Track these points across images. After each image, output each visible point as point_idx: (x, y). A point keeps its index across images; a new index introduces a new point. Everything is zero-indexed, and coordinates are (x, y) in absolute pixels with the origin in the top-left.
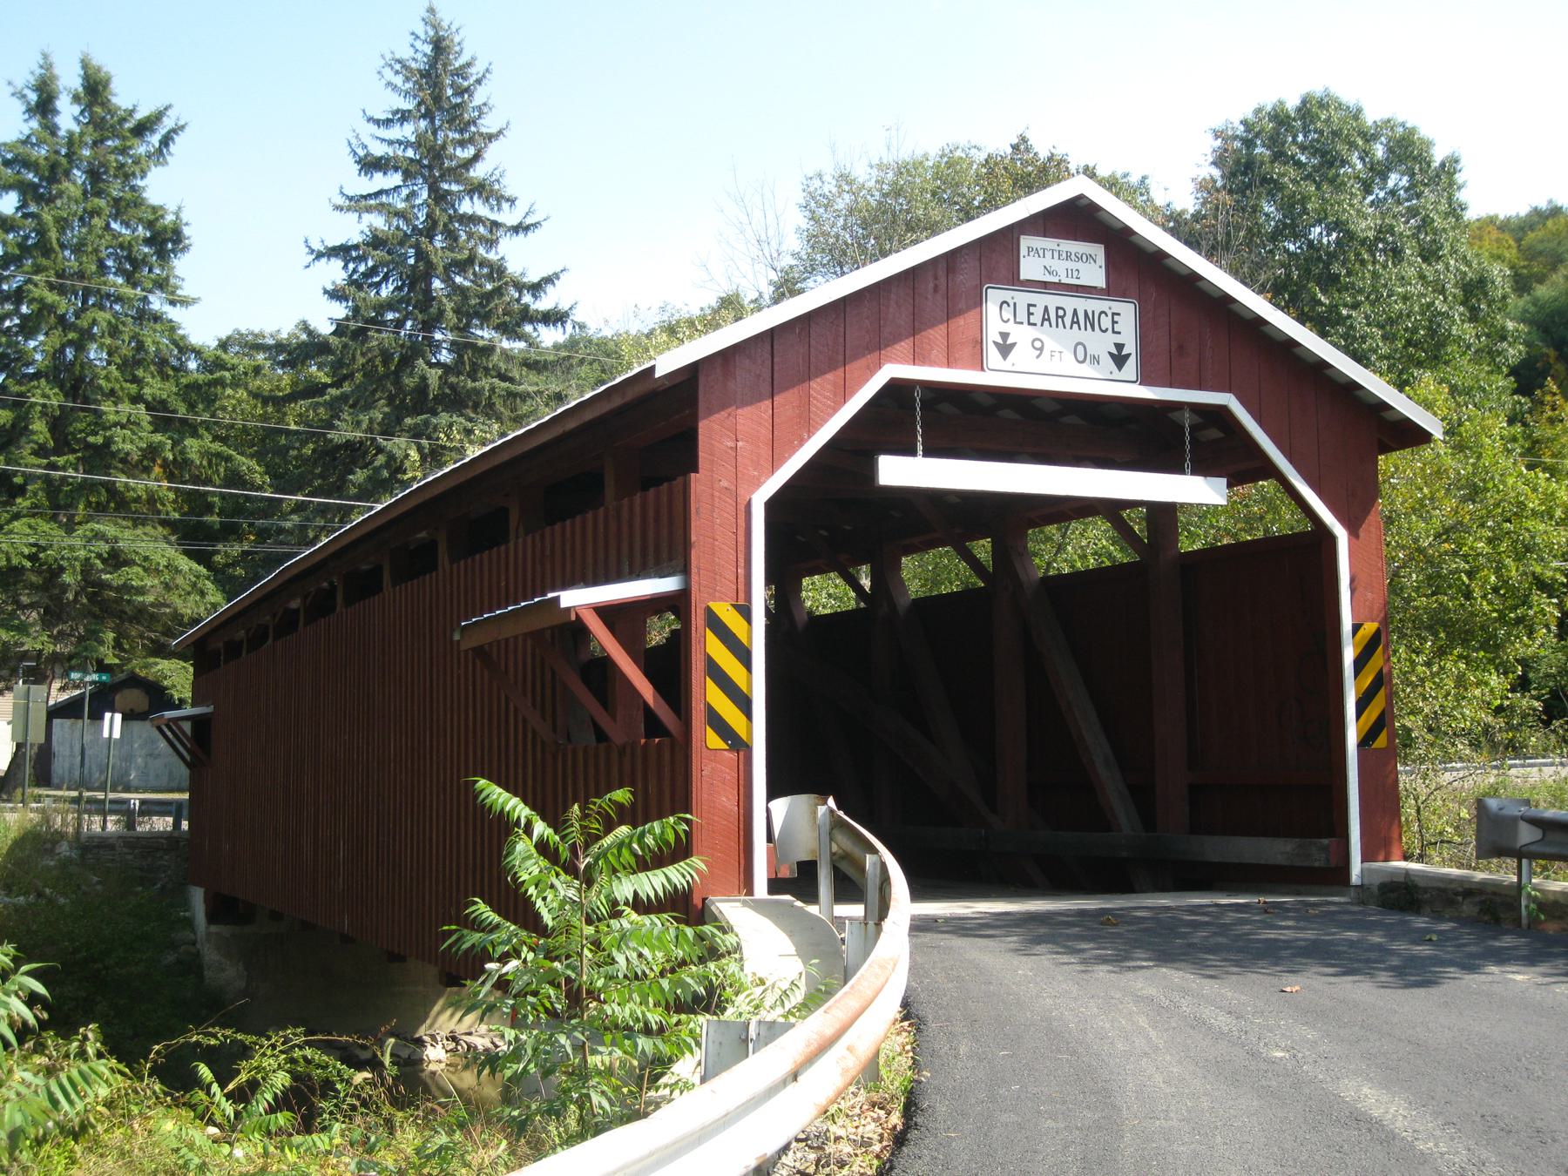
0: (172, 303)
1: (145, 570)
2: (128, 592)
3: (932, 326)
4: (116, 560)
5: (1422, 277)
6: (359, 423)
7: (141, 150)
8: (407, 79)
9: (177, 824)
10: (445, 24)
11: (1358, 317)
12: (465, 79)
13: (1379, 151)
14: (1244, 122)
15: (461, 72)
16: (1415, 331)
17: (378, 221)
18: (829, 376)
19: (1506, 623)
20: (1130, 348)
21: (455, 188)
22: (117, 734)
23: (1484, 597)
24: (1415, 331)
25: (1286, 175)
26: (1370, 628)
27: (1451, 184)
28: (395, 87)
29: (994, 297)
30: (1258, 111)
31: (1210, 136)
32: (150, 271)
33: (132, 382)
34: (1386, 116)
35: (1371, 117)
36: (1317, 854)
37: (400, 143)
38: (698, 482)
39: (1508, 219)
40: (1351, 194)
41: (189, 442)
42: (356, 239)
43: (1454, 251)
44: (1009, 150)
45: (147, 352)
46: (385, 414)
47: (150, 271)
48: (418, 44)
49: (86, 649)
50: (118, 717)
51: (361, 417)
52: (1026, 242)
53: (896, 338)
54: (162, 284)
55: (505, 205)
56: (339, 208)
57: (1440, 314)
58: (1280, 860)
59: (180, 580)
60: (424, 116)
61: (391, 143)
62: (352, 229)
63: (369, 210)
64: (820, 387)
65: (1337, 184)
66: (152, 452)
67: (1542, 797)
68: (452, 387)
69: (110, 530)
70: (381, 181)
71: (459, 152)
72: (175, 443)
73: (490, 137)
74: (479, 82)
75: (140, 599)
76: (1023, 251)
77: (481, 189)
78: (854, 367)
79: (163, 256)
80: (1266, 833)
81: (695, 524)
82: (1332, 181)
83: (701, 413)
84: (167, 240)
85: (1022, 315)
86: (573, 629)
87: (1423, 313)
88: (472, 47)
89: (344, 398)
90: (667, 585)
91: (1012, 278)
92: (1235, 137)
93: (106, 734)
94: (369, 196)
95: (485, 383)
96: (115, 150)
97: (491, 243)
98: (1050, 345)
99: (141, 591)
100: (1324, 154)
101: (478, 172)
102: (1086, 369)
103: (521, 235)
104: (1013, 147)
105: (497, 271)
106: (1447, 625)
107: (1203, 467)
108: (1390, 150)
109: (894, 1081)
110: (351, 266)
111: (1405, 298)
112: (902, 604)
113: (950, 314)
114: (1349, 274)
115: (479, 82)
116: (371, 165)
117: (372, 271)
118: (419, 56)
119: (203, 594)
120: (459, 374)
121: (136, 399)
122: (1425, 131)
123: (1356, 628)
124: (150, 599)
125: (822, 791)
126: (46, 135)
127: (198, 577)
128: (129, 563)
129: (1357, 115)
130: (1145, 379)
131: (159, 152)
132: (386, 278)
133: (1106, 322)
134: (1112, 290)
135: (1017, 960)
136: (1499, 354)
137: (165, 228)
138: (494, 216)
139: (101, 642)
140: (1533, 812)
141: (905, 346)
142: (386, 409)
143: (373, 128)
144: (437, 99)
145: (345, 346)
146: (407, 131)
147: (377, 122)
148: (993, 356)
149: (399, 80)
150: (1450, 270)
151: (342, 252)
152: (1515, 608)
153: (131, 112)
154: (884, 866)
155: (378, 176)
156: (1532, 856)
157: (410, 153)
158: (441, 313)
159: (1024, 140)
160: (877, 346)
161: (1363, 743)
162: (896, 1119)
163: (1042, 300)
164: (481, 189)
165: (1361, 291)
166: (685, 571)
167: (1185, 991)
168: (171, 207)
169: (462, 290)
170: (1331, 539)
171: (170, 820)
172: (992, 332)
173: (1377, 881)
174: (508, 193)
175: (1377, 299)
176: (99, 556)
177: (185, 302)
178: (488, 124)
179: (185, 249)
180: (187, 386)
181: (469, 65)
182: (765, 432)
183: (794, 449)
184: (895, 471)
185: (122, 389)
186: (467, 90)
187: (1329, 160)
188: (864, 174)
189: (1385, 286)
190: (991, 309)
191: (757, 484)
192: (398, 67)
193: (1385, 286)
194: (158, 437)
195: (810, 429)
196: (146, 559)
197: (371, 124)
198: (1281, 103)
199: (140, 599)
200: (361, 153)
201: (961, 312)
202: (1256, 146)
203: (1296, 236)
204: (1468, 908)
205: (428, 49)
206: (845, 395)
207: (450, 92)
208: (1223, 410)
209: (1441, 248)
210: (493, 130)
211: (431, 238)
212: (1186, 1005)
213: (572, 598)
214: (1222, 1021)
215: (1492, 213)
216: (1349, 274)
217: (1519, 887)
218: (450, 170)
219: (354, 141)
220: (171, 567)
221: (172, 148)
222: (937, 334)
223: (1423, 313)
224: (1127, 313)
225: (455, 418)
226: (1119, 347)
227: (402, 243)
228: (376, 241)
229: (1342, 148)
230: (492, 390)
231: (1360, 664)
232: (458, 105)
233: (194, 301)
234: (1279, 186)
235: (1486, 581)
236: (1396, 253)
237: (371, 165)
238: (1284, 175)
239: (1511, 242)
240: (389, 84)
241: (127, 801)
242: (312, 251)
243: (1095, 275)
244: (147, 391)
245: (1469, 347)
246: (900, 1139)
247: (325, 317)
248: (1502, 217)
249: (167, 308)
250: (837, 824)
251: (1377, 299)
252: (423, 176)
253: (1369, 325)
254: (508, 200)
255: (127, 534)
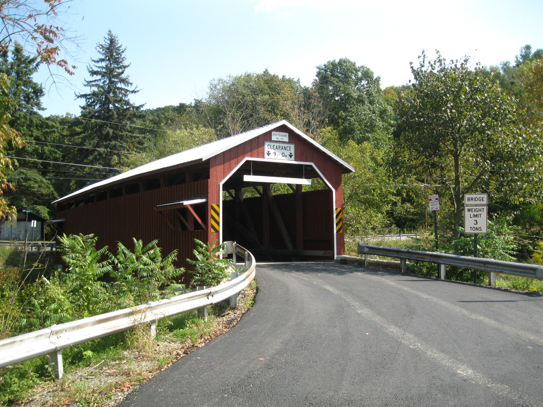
0: (39, 109)
1: (34, 182)
2: (30, 188)
3: (255, 149)
4: (27, 179)
5: (369, 109)
6: (91, 143)
7: (31, 67)
8: (103, 50)
9: (52, 249)
10: (114, 35)
11: (352, 119)
12: (119, 51)
13: (360, 74)
14: (325, 65)
15: (118, 49)
16: (367, 123)
17: (95, 89)
18: (235, 160)
19: (382, 202)
20: (293, 154)
21: (116, 80)
22: (35, 226)
23: (377, 196)
24: (367, 123)
25: (335, 80)
26: (339, 209)
27: (378, 84)
28: (100, 52)
29: (267, 144)
30: (329, 62)
31: (316, 68)
32: (34, 101)
33: (30, 131)
34: (362, 65)
35: (358, 65)
36: (328, 254)
37: (101, 67)
38: (210, 181)
39: (397, 88)
40: (352, 86)
41: (45, 148)
42: (89, 93)
43: (378, 101)
44: (263, 73)
45: (33, 123)
46: (98, 141)
47: (34, 101)
48: (106, 40)
49: (18, 203)
50: (35, 221)
51: (91, 142)
52: (273, 133)
53: (248, 152)
54: (38, 105)
55: (130, 85)
56: (85, 85)
57: (374, 119)
58: (321, 255)
59: (43, 185)
60: (108, 60)
61: (99, 67)
62: (88, 90)
63: (93, 86)
64: (233, 162)
65: (348, 83)
66: (36, 150)
67: (392, 244)
68: (115, 134)
69: (25, 171)
70: (96, 77)
71: (117, 70)
72: (42, 148)
73: (125, 67)
74: (123, 52)
75: (33, 190)
76: (272, 135)
77: (123, 81)
78: (239, 158)
79: (37, 97)
80: (319, 249)
81: (209, 189)
82: (347, 83)
83: (210, 167)
84: (38, 92)
85: (272, 147)
86: (185, 209)
87: (369, 119)
88: (121, 42)
89: (86, 136)
90: (203, 200)
91: (270, 140)
92: (322, 69)
93: (32, 226)
94: (92, 81)
95: (124, 133)
96: (25, 67)
97: (126, 96)
98: (277, 153)
99: (33, 188)
100: (345, 75)
101: (123, 76)
102: (284, 158)
103: (134, 94)
104: (264, 72)
105: (127, 103)
106: (368, 203)
107: (307, 178)
108: (362, 74)
109: (254, 285)
110: (88, 100)
111: (365, 115)
112: (242, 199)
113: (258, 147)
114: (351, 107)
115: (123, 52)
116: (93, 73)
117: (94, 102)
118: (106, 44)
119: (49, 188)
120: (117, 130)
121: (31, 136)
122: (372, 70)
123: (336, 209)
124: (36, 190)
125: (234, 241)
126: (4, 62)
127: (48, 184)
128: (30, 180)
129: (354, 65)
130: (296, 160)
131: (35, 68)
132: (96, 104)
133: (288, 149)
134: (289, 142)
135: (271, 271)
136: (389, 129)
137: (38, 89)
138: (126, 88)
139: (22, 201)
140: (367, 246)
141: (249, 153)
142: (98, 139)
143: (94, 63)
144: (112, 56)
145: (87, 123)
146: (104, 64)
147: (95, 61)
148: (266, 155)
149: (101, 50)
150: (377, 107)
151: (84, 96)
152: (384, 198)
153: (29, 57)
154: (249, 253)
155: (95, 76)
156: (368, 254)
157: (104, 70)
158: (113, 115)
159: (267, 70)
160: (244, 154)
161: (337, 232)
162: (255, 291)
163: (276, 144)
164: (123, 81)
165: (353, 112)
166: (207, 198)
167: (300, 275)
168: (39, 83)
169: (117, 108)
170: (332, 191)
171: (50, 248)
172: (266, 151)
173: (339, 259)
174: (130, 81)
175: (358, 115)
176: (22, 178)
177: (43, 109)
178: (125, 63)
179: (43, 95)
180: (44, 133)
181: (120, 47)
182: (222, 171)
183: (228, 174)
184: (247, 178)
185: (27, 133)
186: (119, 54)
187: (346, 77)
188: (225, 78)
189: (360, 111)
190: (266, 147)
191: (221, 181)
192: (101, 47)
193: (360, 111)
194: (37, 146)
195: (231, 170)
196: (35, 179)
197: (93, 62)
198: (335, 60)
199: (33, 190)
200: (91, 70)
201: (260, 147)
202: (327, 71)
203: (337, 96)
204: (356, 264)
205: (109, 42)
206: (238, 164)
207: (115, 54)
208: (311, 166)
209: (375, 101)
210: (127, 65)
211: (109, 94)
212: (300, 277)
213: (186, 203)
214: (307, 279)
215: (392, 85)
216: (351, 107)
217: (365, 260)
218: (115, 75)
219: (89, 67)
220: (42, 182)
221: (39, 67)
222: (256, 151)
223: (369, 119)
224: (292, 147)
225: (117, 143)
226: (291, 153)
227: (102, 95)
228: (94, 94)
229: (350, 74)
230: (126, 135)
231: (337, 216)
232: (118, 58)
233: (46, 109)
234: (333, 84)
235: (377, 192)
236: (363, 102)
237: (93, 73)
238: (334, 80)
239: (396, 95)
240: (98, 51)
241: (38, 243)
242: (76, 95)
243: (286, 139)
244: (34, 134)
245: (380, 128)
246: (256, 293)
247: (77, 113)
248: (395, 86)
249: (38, 111)
250: (237, 246)
251: (358, 115)
252: (107, 76)
253: (355, 121)
254: (130, 84)
255: (29, 172)
